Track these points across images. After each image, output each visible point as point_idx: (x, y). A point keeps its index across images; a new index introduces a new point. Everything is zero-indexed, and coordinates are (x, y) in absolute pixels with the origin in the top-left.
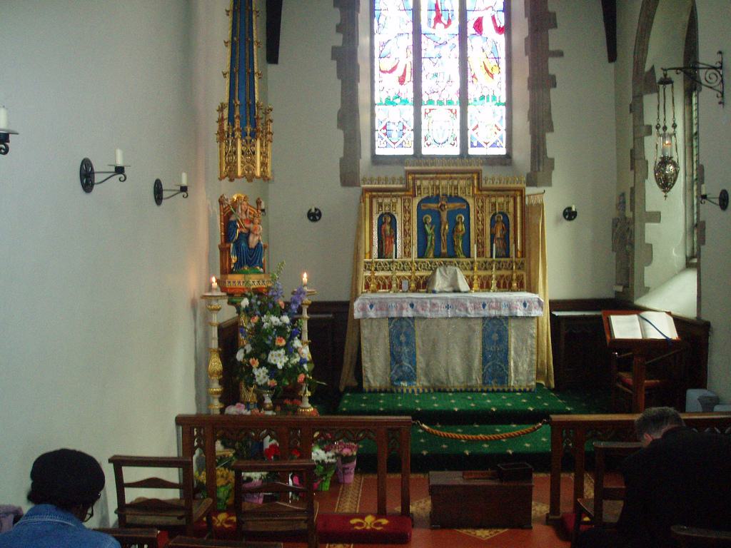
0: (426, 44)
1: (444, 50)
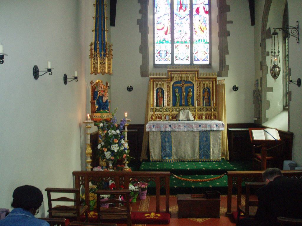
0: (176, 18)
1: (184, 21)
